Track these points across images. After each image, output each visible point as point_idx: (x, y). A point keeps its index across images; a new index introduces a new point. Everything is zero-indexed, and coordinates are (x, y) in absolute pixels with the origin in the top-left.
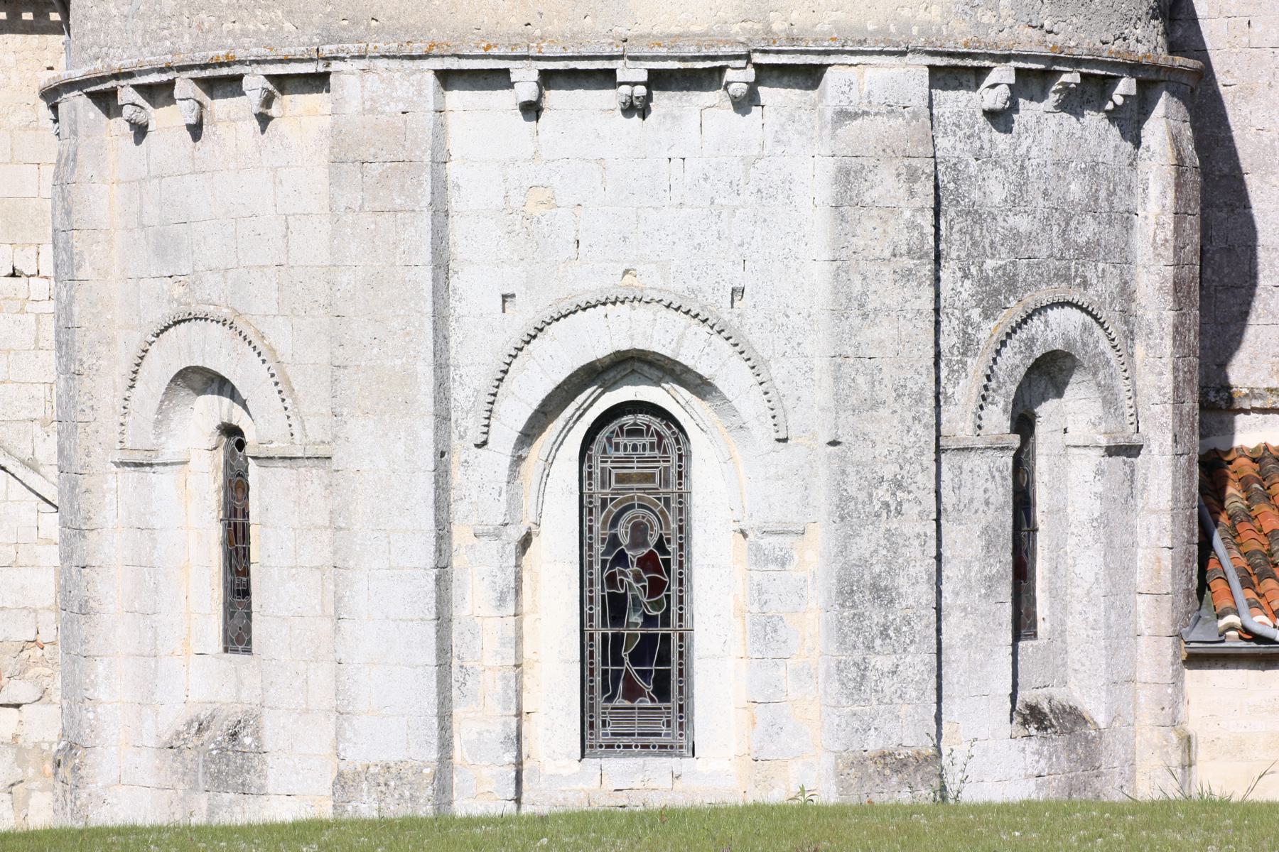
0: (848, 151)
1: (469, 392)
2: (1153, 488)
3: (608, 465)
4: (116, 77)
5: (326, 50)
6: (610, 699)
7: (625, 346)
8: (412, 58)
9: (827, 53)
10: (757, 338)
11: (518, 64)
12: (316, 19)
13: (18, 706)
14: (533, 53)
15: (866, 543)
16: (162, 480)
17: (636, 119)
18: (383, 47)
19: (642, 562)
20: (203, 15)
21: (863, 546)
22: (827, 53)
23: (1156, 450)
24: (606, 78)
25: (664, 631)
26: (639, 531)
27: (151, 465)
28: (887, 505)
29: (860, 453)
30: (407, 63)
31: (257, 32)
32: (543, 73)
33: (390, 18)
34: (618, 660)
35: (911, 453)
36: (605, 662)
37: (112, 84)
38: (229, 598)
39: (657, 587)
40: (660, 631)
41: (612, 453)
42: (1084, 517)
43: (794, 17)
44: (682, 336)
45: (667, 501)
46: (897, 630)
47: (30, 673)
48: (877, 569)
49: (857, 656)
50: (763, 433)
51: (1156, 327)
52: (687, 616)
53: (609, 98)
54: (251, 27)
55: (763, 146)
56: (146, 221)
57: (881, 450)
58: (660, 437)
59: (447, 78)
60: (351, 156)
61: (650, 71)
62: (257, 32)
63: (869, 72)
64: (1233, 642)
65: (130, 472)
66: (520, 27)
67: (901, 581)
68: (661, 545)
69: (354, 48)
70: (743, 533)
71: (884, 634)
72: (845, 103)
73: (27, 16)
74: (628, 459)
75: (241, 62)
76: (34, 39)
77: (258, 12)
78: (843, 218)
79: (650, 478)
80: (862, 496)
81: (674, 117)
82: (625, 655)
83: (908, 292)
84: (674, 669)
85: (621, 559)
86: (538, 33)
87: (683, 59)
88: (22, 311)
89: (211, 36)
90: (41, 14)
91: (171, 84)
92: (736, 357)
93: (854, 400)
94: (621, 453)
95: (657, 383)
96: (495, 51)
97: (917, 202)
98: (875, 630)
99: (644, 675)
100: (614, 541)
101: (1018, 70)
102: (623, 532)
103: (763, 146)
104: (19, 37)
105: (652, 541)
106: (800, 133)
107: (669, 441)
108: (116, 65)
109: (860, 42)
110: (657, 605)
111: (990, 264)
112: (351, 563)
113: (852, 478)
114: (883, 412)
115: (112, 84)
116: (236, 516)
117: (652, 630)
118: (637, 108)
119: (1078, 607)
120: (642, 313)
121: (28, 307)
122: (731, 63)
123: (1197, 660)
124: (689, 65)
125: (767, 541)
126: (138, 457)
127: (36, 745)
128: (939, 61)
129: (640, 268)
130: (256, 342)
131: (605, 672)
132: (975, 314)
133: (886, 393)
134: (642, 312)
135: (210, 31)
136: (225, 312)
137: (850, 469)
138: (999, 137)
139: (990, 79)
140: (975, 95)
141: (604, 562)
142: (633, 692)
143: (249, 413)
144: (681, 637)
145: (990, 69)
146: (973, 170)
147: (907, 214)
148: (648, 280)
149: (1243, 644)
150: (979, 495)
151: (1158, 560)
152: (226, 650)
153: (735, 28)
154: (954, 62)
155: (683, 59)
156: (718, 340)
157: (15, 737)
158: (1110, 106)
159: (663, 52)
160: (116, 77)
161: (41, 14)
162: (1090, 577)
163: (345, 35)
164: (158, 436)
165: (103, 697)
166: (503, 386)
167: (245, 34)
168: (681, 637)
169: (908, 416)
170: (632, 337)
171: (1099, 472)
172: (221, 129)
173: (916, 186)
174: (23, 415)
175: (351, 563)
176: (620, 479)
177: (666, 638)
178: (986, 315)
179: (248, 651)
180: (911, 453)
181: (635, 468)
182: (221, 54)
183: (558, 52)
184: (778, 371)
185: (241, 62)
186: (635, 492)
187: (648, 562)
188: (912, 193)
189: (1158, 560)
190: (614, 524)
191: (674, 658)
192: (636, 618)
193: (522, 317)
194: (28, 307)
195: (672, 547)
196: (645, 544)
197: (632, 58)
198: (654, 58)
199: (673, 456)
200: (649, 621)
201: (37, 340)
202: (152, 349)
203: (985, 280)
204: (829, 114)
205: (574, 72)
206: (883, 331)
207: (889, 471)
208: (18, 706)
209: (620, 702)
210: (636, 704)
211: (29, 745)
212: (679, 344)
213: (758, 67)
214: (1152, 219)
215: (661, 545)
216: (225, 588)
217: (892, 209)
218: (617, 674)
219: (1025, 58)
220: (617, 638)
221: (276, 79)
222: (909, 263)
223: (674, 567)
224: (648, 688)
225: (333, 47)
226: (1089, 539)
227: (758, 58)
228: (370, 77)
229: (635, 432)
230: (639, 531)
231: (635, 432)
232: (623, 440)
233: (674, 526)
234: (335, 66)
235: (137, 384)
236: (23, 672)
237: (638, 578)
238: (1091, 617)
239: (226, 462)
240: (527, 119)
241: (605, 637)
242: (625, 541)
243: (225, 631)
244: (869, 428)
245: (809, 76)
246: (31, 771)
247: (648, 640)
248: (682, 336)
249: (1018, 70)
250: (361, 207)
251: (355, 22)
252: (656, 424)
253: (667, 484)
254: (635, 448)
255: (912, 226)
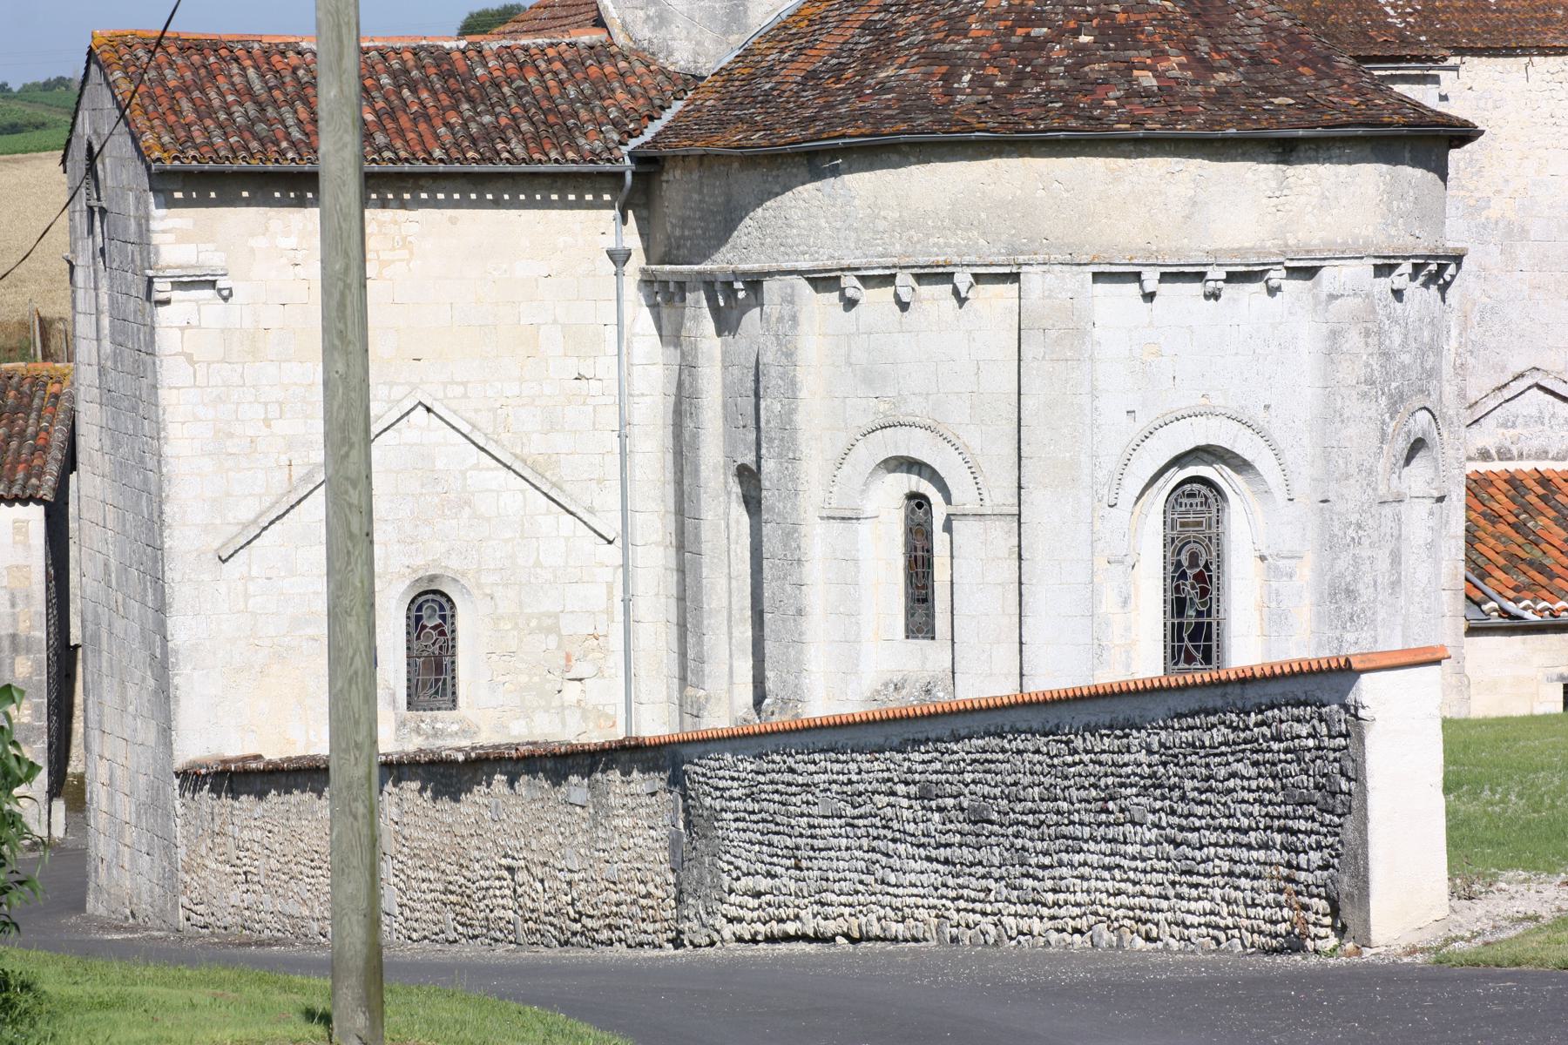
0: (1335, 319)
1: (1105, 472)
2: (1453, 523)
3: (1176, 516)
4: (842, 270)
5: (1021, 259)
6: (1176, 664)
7: (1203, 443)
8: (1079, 265)
9: (1324, 259)
10: (1276, 435)
11: (1148, 268)
12: (1004, 237)
13: (580, 680)
14: (1160, 262)
15: (1343, 563)
16: (863, 528)
17: (1212, 301)
18: (1060, 258)
19: (1196, 577)
20: (912, 232)
21: (1343, 563)
22: (1324, 259)
23: (1454, 498)
24: (1200, 277)
25: (1208, 620)
26: (1194, 558)
27: (858, 519)
28: (1353, 539)
29: (1339, 507)
30: (1075, 268)
31: (957, 245)
32: (1163, 274)
33: (1057, 238)
34: (1181, 639)
35: (1365, 507)
36: (1173, 641)
37: (839, 273)
38: (910, 604)
39: (1204, 592)
40: (1206, 620)
41: (1178, 509)
42: (1421, 542)
43: (1300, 235)
44: (1236, 436)
45: (1210, 538)
46: (1358, 616)
47: (590, 657)
48: (1348, 579)
49: (1338, 633)
50: (1280, 495)
51: (1455, 420)
52: (1222, 611)
53: (1197, 288)
54: (953, 241)
55: (1282, 317)
56: (853, 360)
57: (1351, 505)
58: (1206, 498)
59: (1098, 277)
60: (1037, 326)
61: (1228, 273)
62: (957, 245)
63: (1344, 270)
64: (1495, 619)
65: (836, 524)
66: (1144, 245)
67: (1361, 586)
68: (1207, 567)
69: (1040, 258)
70: (1263, 558)
71: (1351, 619)
72: (1332, 291)
73: (589, 197)
74: (1187, 512)
75: (955, 265)
76: (593, 213)
77: (959, 232)
78: (1332, 362)
79: (1199, 524)
80: (1341, 534)
81: (1234, 300)
82: (1185, 636)
83: (1364, 406)
84: (1214, 644)
85: (1183, 575)
86: (1154, 248)
87: (1248, 265)
88: (584, 403)
89: (919, 247)
90: (598, 196)
91: (894, 276)
92: (1267, 449)
93: (1337, 475)
94: (1183, 509)
95: (1210, 465)
96: (1136, 261)
97: (1370, 350)
98: (1347, 617)
99: (1196, 648)
100: (1179, 564)
101: (1414, 265)
102: (1184, 558)
103: (1282, 317)
104: (583, 212)
105: (1202, 563)
106: (1302, 308)
107: (1211, 500)
108: (845, 263)
109: (1343, 252)
110: (1203, 605)
111: (1394, 385)
112: (1034, 581)
113: (1336, 523)
114: (1352, 481)
115: (839, 273)
116: (916, 550)
117: (1201, 620)
118: (1214, 296)
119: (1417, 599)
120: (1214, 422)
121: (589, 400)
122: (1275, 267)
123: (1472, 631)
124: (1250, 269)
125: (1281, 563)
126: (848, 514)
127: (595, 707)
128: (1379, 262)
129: (1212, 394)
130: (954, 440)
131: (1173, 647)
132: (1387, 417)
133: (1353, 470)
134: (1214, 421)
135: (919, 242)
136: (929, 422)
137: (1335, 517)
138: (1398, 305)
139: (1398, 271)
140: (1388, 280)
141: (1173, 577)
142: (1190, 659)
143: (1138, 499)
144: (1218, 624)
145: (1399, 265)
146: (1387, 327)
147: (1365, 357)
148: (1217, 401)
149: (1501, 620)
150: (1388, 530)
151: (1456, 568)
152: (907, 637)
153: (1269, 244)
154: (1387, 261)
155: (1248, 265)
156: (1257, 438)
157: (579, 701)
158: (1441, 282)
159: (1238, 261)
160: (842, 270)
161: (598, 196)
162: (1425, 580)
163: (1025, 248)
164: (862, 500)
165: (814, 669)
166: (1127, 469)
167: (947, 245)
168: (1218, 624)
169: (1365, 483)
170: (1207, 437)
171: (1431, 513)
172: (926, 305)
173: (1370, 340)
174: (585, 476)
175: (1034, 581)
176: (1183, 525)
177: (1210, 624)
178: (1392, 418)
179: (933, 638)
180: (1365, 507)
181: (1191, 518)
182: (941, 259)
183: (1175, 261)
184: (1288, 457)
185: (955, 265)
186: (1191, 532)
187: (1199, 577)
188: (1367, 344)
189: (1456, 568)
190: (1179, 553)
191: (1214, 637)
192: (1192, 613)
193: (1143, 422)
194: (589, 400)
195: (1213, 567)
196: (1198, 566)
197: (1218, 265)
198: (1231, 265)
199: (1214, 510)
200: (1200, 614)
201: (594, 424)
202: (860, 445)
203: (1391, 396)
204: (1323, 296)
205: (1183, 273)
206: (1352, 430)
207: (1354, 518)
208: (580, 680)
209: (1182, 665)
210: (1192, 666)
211: (590, 708)
212: (1235, 441)
213: (1287, 268)
214: (1453, 351)
215: (1207, 567)
216: (907, 598)
217: (1357, 355)
218: (1180, 648)
219: (1416, 257)
220: (1181, 625)
221: (975, 276)
222: (1365, 388)
223: (1214, 580)
224: (1199, 656)
225: (1026, 257)
226: (1424, 556)
227: (1289, 264)
228: (1049, 276)
229: (1191, 495)
230: (1194, 558)
231: (1191, 495)
232: (1184, 500)
233: (1214, 554)
234: (1024, 269)
235: (844, 466)
236: (585, 656)
237: (1193, 587)
238: (1425, 605)
239: (907, 517)
240: (1145, 301)
241: (1173, 624)
242: (1186, 563)
243: (907, 626)
244: (1345, 491)
245: (1309, 273)
246: (591, 725)
247: (1199, 626)
248: (1236, 436)
249: (1414, 265)
250: (1044, 357)
251: (1031, 240)
252: (1204, 490)
253: (1210, 527)
254: (1191, 505)
255: (1367, 365)
